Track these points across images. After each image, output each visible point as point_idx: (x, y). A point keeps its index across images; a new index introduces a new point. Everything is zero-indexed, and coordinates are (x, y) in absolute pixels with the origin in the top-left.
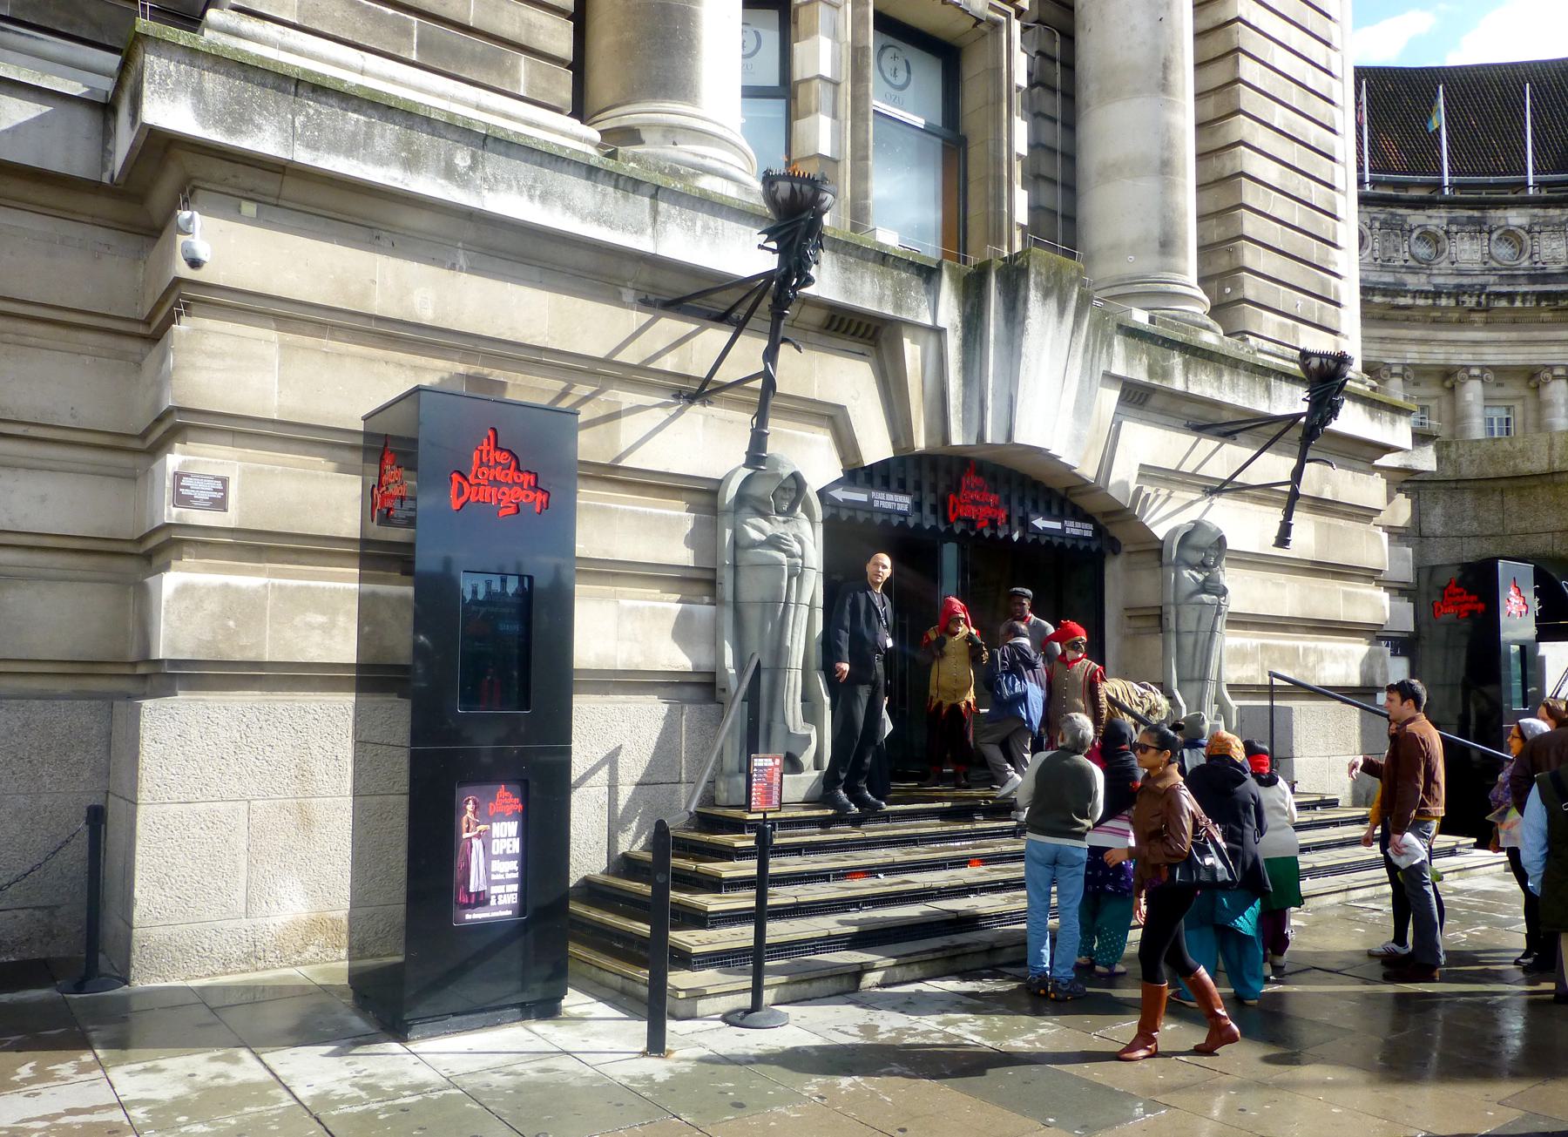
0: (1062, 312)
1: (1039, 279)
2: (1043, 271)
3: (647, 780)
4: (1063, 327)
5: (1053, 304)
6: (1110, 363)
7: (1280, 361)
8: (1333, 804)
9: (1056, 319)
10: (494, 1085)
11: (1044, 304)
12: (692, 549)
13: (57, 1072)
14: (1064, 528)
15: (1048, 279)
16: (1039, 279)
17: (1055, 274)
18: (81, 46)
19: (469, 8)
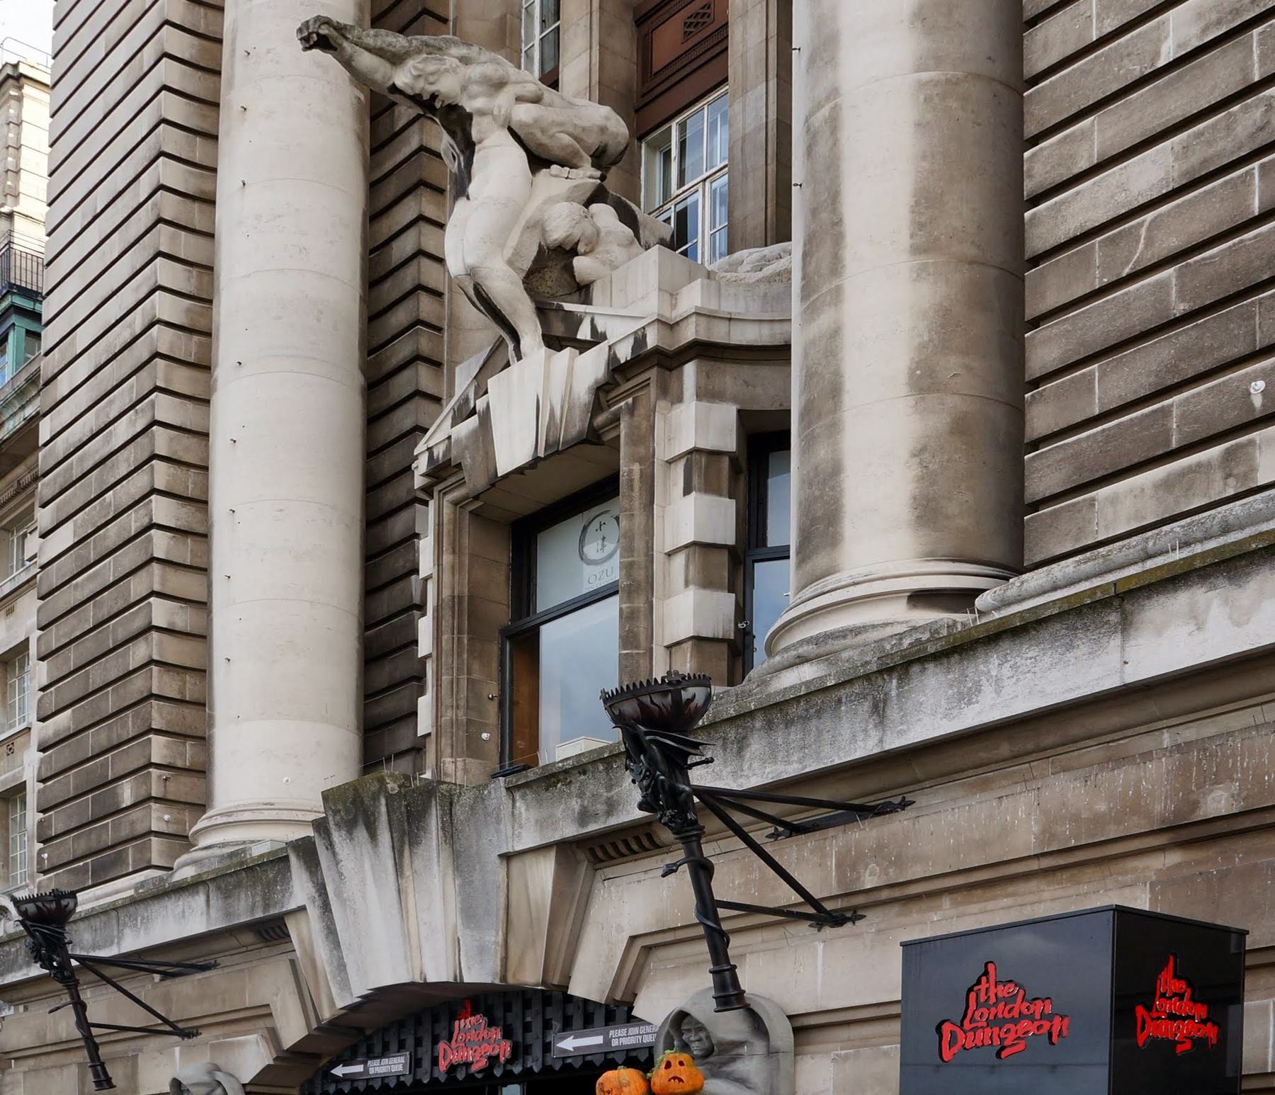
0: (373, 835)
1: (338, 818)
2: (340, 807)
3: (723, 55)
4: (381, 849)
5: (361, 833)
6: (571, 372)
7: (594, 14)
8: (681, 182)
9: (369, 847)
10: (1221, 578)
11: (352, 839)
12: (54, 734)
13: (658, 160)
14: (608, 1041)
15: (347, 811)
16: (338, 818)
17: (354, 802)
18: (119, 422)
19: (90, 553)
